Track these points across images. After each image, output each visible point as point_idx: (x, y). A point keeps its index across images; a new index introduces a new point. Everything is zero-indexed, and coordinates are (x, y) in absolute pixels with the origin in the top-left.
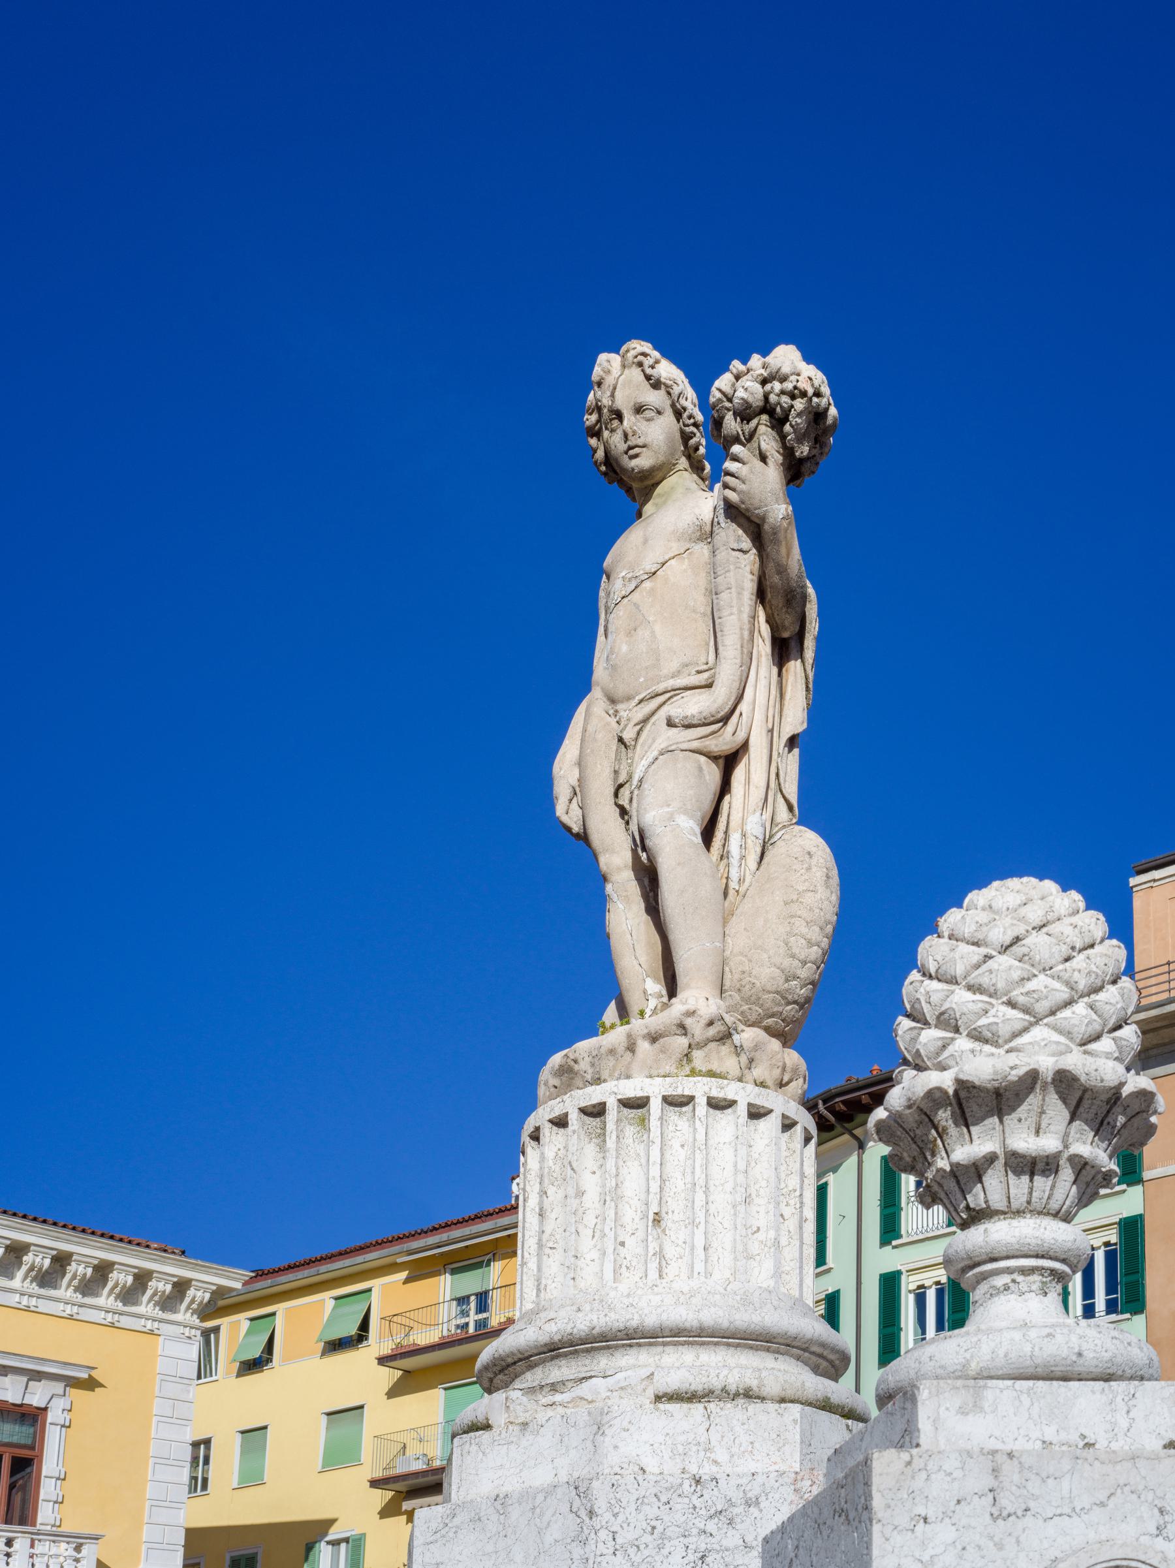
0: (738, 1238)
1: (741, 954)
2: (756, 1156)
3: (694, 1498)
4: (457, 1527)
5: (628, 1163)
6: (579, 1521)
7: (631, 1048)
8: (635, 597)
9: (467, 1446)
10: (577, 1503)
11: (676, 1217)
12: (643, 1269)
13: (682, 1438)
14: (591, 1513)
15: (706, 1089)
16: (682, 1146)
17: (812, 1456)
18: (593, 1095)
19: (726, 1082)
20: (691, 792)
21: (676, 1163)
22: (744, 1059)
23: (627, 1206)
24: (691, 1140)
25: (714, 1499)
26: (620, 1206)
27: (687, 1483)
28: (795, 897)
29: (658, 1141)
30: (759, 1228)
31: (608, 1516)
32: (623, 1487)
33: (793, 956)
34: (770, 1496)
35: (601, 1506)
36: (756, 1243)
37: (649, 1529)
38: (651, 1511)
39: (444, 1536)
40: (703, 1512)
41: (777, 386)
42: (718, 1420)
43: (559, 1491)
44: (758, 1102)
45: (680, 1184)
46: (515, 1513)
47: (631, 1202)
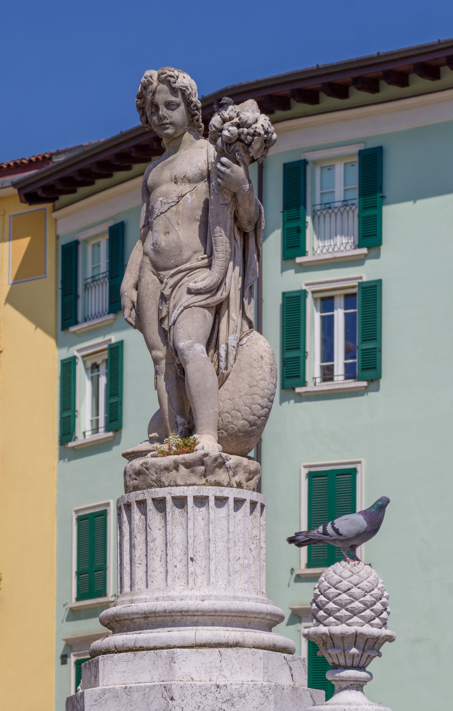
0: (230, 564)
1: (227, 412)
2: (238, 521)
3: (216, 694)
4: (106, 699)
5: (177, 527)
6: (166, 702)
7: (176, 468)
8: (168, 214)
9: (106, 661)
10: (165, 694)
11: (201, 554)
12: (186, 579)
13: (209, 665)
14: (172, 699)
15: (214, 492)
16: (203, 519)
17: (268, 673)
18: (160, 492)
19: (223, 488)
20: (201, 330)
21: (200, 528)
22: (231, 473)
23: (177, 548)
24: (207, 517)
25: (225, 694)
26: (174, 548)
27: (213, 687)
28: (255, 384)
29: (192, 518)
30: (239, 558)
31: (179, 701)
32: (185, 688)
33: (254, 415)
34: (250, 694)
35: (176, 696)
36: (238, 565)
37: (197, 707)
38: (198, 699)
39: (99, 703)
40: (220, 700)
41: (245, 130)
42: (225, 657)
43: (157, 688)
44: (239, 496)
45: (202, 537)
46: (135, 695)
47: (179, 546)
